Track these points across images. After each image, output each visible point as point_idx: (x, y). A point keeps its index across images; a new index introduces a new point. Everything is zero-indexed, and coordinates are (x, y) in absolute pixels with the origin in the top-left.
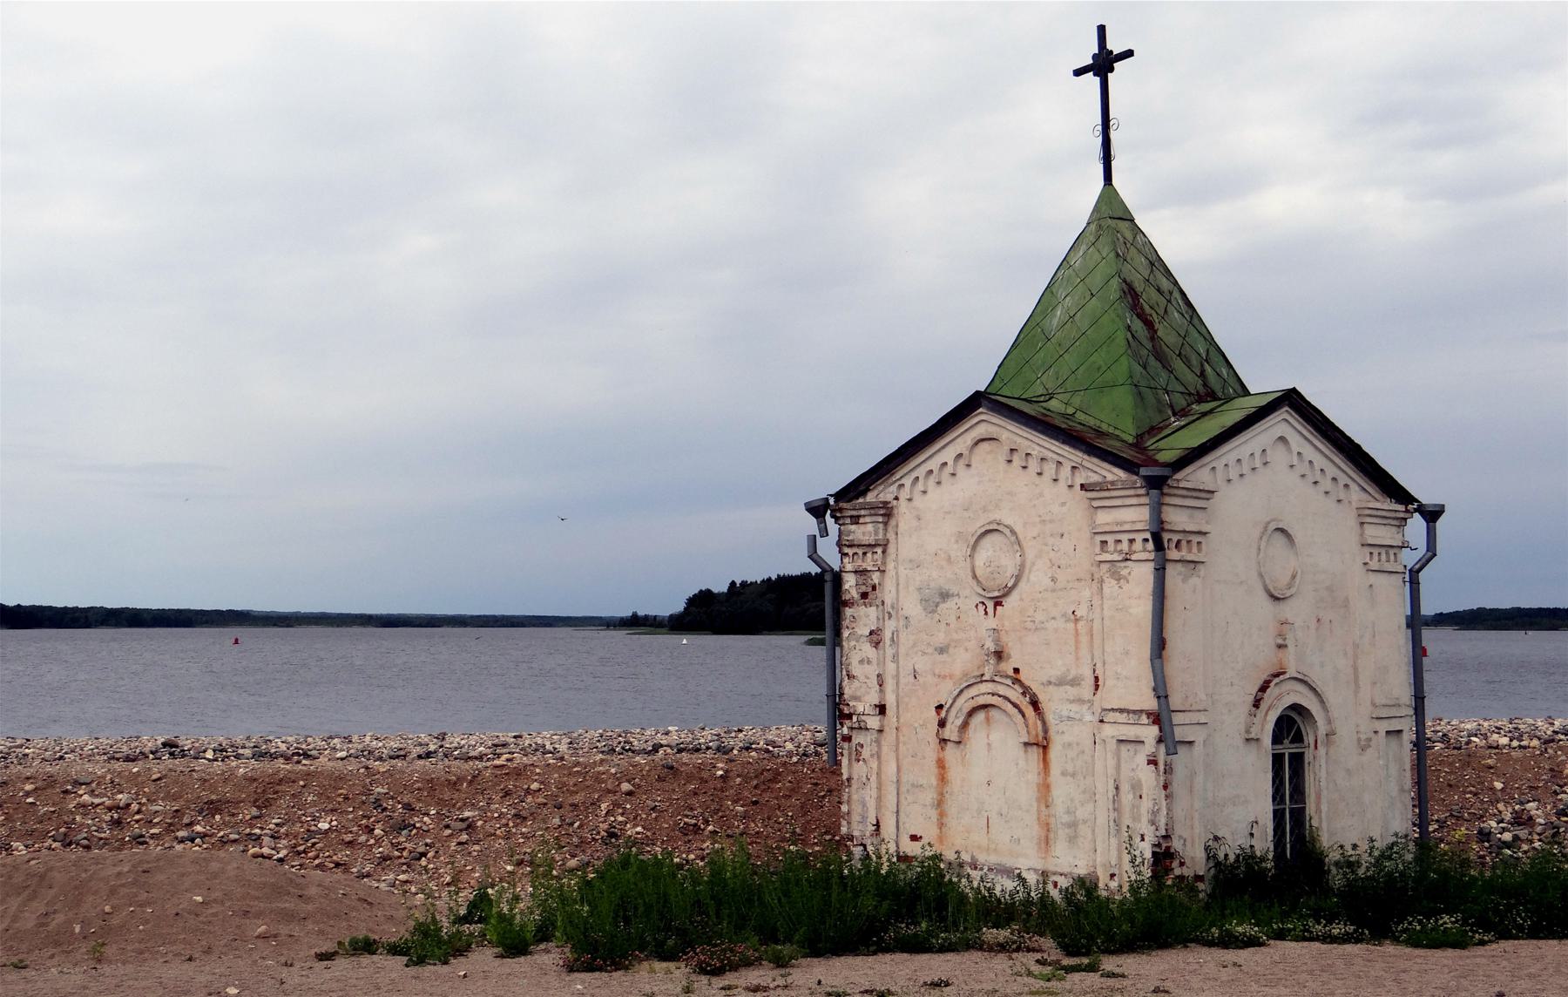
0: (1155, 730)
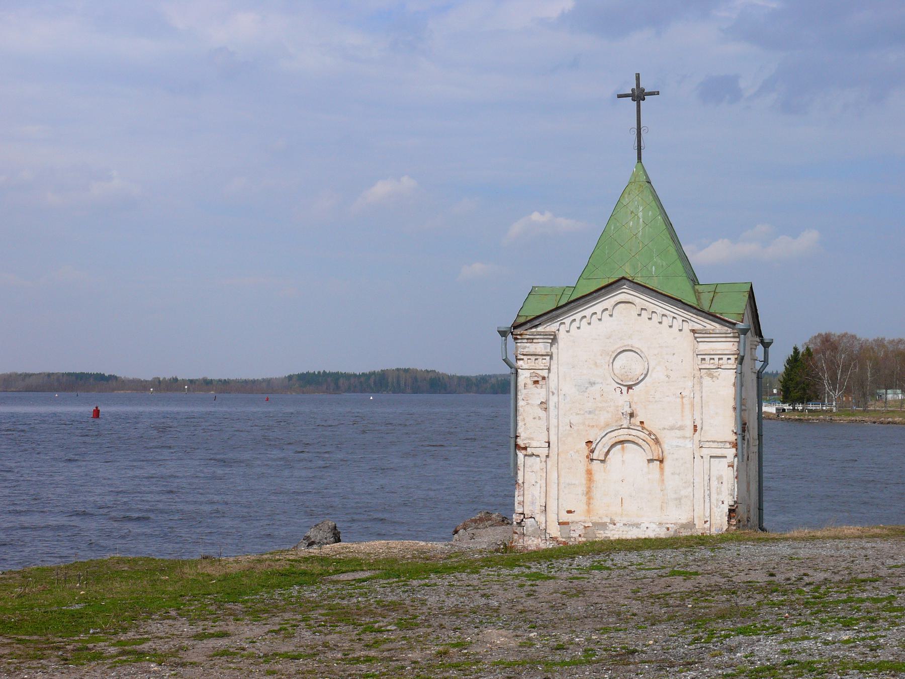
0: (734, 450)
